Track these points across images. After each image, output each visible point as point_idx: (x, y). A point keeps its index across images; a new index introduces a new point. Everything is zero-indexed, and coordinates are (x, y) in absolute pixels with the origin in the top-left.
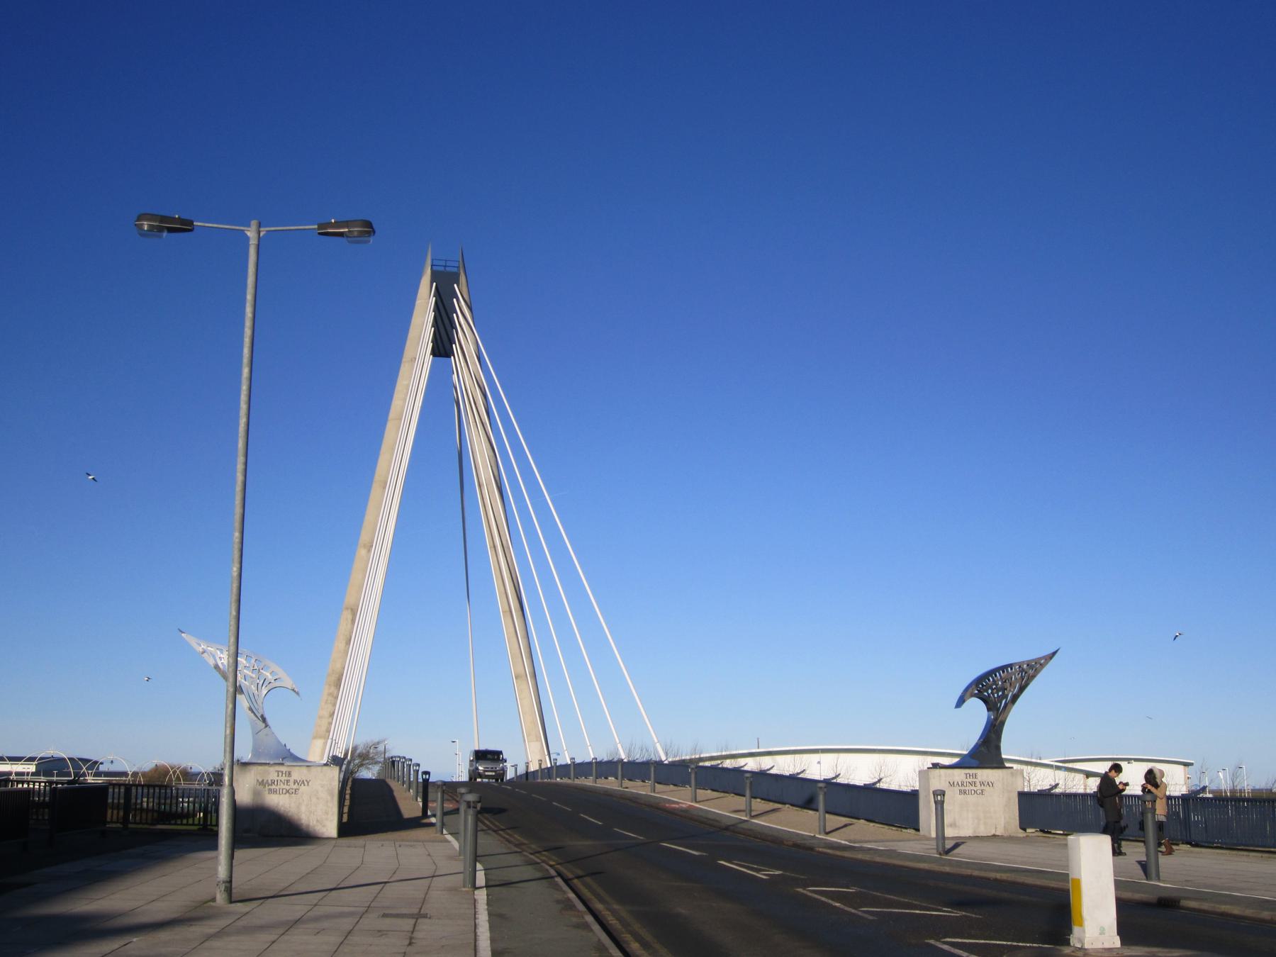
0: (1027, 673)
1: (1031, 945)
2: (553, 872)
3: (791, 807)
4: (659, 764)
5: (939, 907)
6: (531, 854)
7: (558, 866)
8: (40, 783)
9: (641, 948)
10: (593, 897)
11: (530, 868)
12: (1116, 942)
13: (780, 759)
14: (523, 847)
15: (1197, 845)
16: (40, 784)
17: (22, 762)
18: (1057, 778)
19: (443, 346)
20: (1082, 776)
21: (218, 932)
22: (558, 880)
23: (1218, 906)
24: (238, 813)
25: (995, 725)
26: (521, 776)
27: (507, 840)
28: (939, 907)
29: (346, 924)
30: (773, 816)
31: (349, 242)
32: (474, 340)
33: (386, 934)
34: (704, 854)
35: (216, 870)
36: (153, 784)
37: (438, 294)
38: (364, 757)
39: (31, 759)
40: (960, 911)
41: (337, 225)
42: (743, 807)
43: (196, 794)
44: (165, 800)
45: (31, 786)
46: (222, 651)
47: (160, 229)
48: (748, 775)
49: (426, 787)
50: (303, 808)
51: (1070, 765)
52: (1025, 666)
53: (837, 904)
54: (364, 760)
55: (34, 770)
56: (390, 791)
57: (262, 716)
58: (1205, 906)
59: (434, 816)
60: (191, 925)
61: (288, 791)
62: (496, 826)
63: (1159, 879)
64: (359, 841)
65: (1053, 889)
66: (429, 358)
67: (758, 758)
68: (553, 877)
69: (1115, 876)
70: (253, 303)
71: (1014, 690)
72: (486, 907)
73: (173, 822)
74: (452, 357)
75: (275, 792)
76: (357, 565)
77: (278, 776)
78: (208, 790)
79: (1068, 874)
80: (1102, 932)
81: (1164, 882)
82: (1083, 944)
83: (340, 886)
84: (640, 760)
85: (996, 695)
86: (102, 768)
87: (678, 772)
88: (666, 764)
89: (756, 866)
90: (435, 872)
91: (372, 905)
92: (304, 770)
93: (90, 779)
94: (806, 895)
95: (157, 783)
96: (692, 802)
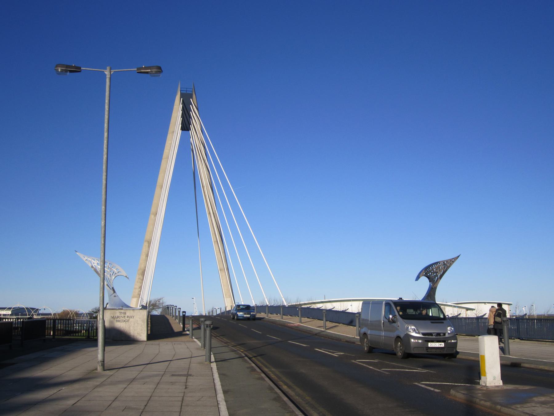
0: (446, 265)
1: (460, 384)
2: (244, 355)
3: (343, 325)
4: (284, 307)
5: (416, 368)
6: (232, 347)
7: (245, 352)
8: (13, 319)
9: (288, 388)
10: (262, 366)
11: (233, 353)
12: (500, 383)
13: (334, 304)
14: (228, 344)
15: (522, 339)
16: (13, 319)
17: (6, 310)
18: (454, 311)
19: (186, 126)
20: (465, 310)
21: (100, 384)
22: (246, 358)
23: (538, 366)
24: (106, 331)
25: (433, 288)
26: (223, 313)
27: (221, 341)
28: (416, 368)
29: (157, 379)
30: (336, 328)
31: (151, 76)
32: (200, 123)
33: (175, 384)
34: (308, 346)
35: (97, 357)
36: (63, 318)
37: (184, 103)
38: (153, 305)
39: (10, 309)
40: (426, 370)
41: (145, 68)
42: (322, 325)
43: (82, 323)
44: (68, 325)
45: (9, 320)
46: (94, 260)
47: (66, 71)
48: (324, 311)
49: (184, 318)
50: (131, 328)
51: (460, 305)
52: (446, 262)
53: (371, 367)
54: (154, 307)
55: (11, 313)
56: (168, 320)
57: (113, 288)
58: (533, 366)
59: (188, 330)
60: (88, 381)
61: (124, 321)
62: (215, 335)
63: (509, 354)
64: (157, 342)
65: (463, 359)
66: (180, 131)
67: (325, 304)
68: (243, 357)
69: (500, 354)
70: (108, 104)
71: (441, 273)
72: (217, 371)
73: (72, 335)
74: (190, 131)
75: (119, 321)
76: (150, 222)
77: (120, 314)
78: (89, 321)
79: (479, 354)
80: (494, 379)
81: (512, 355)
82: (486, 384)
83: (151, 362)
84: (275, 305)
85: (433, 275)
86: (40, 312)
87: (293, 310)
88: (287, 307)
89: (332, 351)
90: (192, 355)
91: (166, 371)
92: (132, 311)
93: (35, 317)
94: (356, 363)
95: (64, 318)
96: (299, 323)
